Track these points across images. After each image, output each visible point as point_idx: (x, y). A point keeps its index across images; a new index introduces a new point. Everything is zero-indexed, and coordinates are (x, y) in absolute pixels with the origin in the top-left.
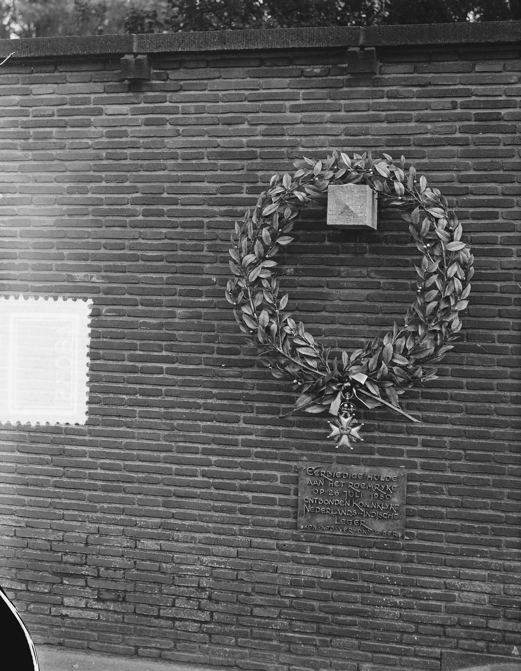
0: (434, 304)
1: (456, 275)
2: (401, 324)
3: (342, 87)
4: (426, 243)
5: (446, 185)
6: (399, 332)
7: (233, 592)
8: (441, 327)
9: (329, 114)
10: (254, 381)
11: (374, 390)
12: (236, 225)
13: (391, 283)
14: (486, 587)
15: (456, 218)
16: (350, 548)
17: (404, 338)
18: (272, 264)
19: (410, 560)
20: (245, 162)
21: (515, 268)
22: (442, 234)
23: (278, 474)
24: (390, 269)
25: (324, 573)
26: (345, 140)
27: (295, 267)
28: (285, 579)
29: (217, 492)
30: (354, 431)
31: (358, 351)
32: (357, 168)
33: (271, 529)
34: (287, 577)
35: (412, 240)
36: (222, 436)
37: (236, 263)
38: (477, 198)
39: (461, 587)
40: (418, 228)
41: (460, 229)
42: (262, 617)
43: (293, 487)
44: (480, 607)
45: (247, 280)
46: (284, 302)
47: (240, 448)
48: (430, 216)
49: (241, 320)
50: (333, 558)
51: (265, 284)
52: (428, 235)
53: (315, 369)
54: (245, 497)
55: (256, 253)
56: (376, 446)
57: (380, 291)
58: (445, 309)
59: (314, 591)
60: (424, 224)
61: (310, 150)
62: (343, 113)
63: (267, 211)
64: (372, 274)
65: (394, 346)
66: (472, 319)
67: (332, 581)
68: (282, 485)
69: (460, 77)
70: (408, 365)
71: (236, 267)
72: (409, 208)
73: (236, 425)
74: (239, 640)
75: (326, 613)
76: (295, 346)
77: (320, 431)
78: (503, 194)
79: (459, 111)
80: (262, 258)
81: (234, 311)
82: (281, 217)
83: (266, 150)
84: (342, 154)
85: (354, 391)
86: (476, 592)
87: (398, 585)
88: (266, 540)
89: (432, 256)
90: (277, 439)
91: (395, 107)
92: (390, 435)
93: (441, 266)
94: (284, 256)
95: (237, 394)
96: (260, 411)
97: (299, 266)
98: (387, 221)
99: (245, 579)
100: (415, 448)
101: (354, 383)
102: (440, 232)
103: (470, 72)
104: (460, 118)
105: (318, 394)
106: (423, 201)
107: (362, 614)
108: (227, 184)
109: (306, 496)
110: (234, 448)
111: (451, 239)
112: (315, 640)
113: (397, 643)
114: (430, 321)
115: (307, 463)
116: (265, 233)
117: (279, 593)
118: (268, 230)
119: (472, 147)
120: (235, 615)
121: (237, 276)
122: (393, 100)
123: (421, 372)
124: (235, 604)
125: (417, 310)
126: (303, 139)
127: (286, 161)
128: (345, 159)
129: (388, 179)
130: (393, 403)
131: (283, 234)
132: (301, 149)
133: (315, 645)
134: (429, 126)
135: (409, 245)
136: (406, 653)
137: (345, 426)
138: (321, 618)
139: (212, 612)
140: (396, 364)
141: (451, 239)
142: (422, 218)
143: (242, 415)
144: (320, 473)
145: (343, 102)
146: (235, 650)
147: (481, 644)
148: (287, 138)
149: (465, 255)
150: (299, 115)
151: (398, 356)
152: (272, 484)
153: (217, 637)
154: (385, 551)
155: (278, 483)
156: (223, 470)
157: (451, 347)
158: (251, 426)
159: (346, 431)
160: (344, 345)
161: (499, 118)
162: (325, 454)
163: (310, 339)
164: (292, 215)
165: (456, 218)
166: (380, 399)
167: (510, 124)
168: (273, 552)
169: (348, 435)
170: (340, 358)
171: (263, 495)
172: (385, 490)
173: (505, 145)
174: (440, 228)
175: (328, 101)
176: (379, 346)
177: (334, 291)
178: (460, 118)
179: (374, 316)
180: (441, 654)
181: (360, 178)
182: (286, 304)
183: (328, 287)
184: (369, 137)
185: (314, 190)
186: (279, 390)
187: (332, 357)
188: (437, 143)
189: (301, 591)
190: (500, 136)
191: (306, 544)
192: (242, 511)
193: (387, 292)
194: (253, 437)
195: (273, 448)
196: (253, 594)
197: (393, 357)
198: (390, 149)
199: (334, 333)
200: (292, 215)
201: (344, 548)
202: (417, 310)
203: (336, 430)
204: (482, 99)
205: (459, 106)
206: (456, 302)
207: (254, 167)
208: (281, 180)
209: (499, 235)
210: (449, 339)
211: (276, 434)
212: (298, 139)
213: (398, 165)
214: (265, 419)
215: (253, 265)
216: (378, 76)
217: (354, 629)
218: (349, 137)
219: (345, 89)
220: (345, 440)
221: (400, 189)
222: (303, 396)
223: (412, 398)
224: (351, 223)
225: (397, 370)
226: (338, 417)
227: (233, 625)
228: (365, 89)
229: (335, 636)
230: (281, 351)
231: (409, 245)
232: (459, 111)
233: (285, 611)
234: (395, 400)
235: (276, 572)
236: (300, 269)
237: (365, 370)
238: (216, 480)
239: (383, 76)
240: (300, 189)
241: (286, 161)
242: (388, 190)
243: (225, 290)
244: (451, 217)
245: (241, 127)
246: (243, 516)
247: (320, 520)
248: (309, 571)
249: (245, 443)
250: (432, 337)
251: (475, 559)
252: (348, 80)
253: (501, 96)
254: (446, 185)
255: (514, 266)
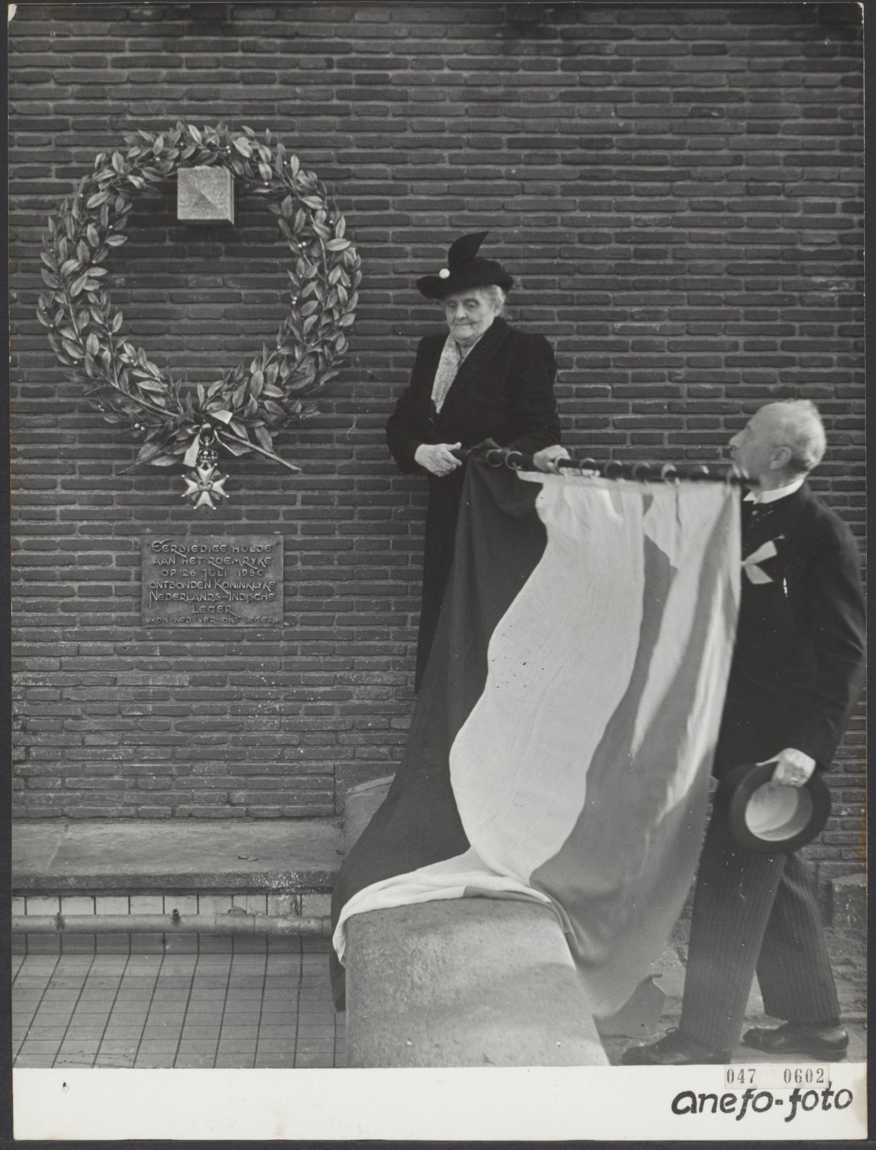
0: (313, 319)
1: (339, 281)
2: (272, 347)
3: (181, 36)
4: (301, 242)
5: (322, 165)
6: (269, 356)
7: (56, 716)
8: (323, 347)
9: (164, 72)
10: (75, 432)
11: (240, 432)
12: (50, 221)
13: (254, 294)
14: (387, 678)
15: (337, 208)
16: (213, 643)
17: (276, 364)
18: (100, 272)
19: (292, 652)
20: (53, 135)
21: (412, 272)
22: (321, 229)
23: (113, 554)
24: (252, 275)
25: (180, 679)
26: (189, 106)
27: (126, 275)
28: (127, 693)
29: (28, 584)
30: (217, 486)
31: (217, 383)
32: (210, 146)
33: (104, 628)
34: (130, 690)
35: (281, 237)
36: (33, 508)
37: (50, 271)
38: (362, 182)
39: (356, 680)
40: (290, 222)
41: (343, 223)
42: (99, 746)
43: (133, 570)
44: (381, 703)
45: (68, 295)
46: (118, 323)
47: (58, 522)
48: (305, 207)
49: (61, 347)
50: (191, 659)
51: (92, 299)
52: (303, 230)
53: (163, 408)
54: (68, 587)
55: (80, 258)
56: (244, 508)
57: (242, 305)
58: (327, 325)
59: (167, 704)
60: (298, 217)
61: (142, 119)
62: (184, 70)
63: (93, 201)
64: (230, 283)
65: (265, 374)
66: (359, 338)
67: (191, 688)
68: (118, 568)
69: (336, 28)
70: (282, 398)
71: (52, 277)
72: (277, 197)
73: (51, 492)
74: (67, 780)
75: (184, 731)
76: (134, 381)
77: (167, 493)
78: (394, 178)
79: (335, 71)
80: (87, 265)
81: (51, 338)
82: (112, 209)
83: (81, 118)
84: (191, 127)
85: (216, 433)
86: (377, 684)
87: (277, 685)
88: (99, 644)
89: (309, 257)
90: (110, 508)
91: (253, 64)
92: (260, 492)
93: (321, 270)
94: (115, 261)
95: (52, 450)
96: (84, 471)
97: (132, 275)
98: (247, 213)
99: (73, 698)
100: (293, 508)
101: (216, 423)
102: (318, 228)
103: (348, 21)
104: (338, 80)
105: (167, 441)
106: (296, 188)
107: (231, 728)
108: (28, 165)
109: (153, 580)
110: (50, 523)
111: (332, 236)
112: (170, 768)
113: (278, 760)
114: (308, 341)
115: (152, 537)
116: (91, 230)
117: (120, 713)
118: (95, 227)
119: (354, 118)
120: (61, 747)
121: (52, 289)
122: (250, 55)
123: (300, 407)
124: (59, 732)
125: (294, 329)
126: (132, 104)
127: (110, 134)
128: (195, 133)
129: (250, 160)
130: (266, 446)
131: (113, 233)
132: (129, 118)
133: (171, 775)
134: (298, 90)
135: (277, 244)
136: (290, 772)
137: (204, 479)
138: (178, 738)
139: (28, 747)
140: (268, 398)
141: (332, 236)
142: (296, 210)
143: (60, 478)
144: (169, 548)
145: (184, 55)
146: (62, 794)
147: (384, 750)
148: (110, 103)
149: (350, 256)
150: (126, 72)
151: (270, 386)
152: (104, 568)
153: (36, 780)
154: (258, 644)
155: (113, 566)
156: (35, 554)
157: (336, 373)
158: (73, 492)
159: (206, 486)
160: (195, 378)
161: (385, 81)
162: (175, 523)
163: (154, 370)
164: (125, 206)
165: (337, 208)
166: (248, 443)
167: (400, 89)
168: (109, 658)
169: (210, 491)
170: (195, 395)
171: (93, 583)
172: (256, 564)
173: (394, 115)
174: (318, 221)
175: (164, 54)
176: (244, 376)
177: (179, 307)
178: (338, 80)
179: (234, 338)
180: (334, 768)
181: (214, 159)
182: (119, 324)
183: (172, 301)
184: (220, 102)
185: (154, 174)
186: (110, 442)
187: (183, 393)
188: (309, 112)
189: (150, 707)
190: (389, 104)
191: (153, 644)
192: (65, 608)
193: (250, 307)
194: (76, 507)
195: (105, 520)
196: (84, 716)
197: (264, 389)
198: (249, 118)
199: (182, 362)
200: (125, 206)
201: (204, 644)
202: (294, 329)
203: (193, 486)
204: (364, 56)
205: (335, 64)
206: (341, 316)
207: (66, 141)
208: (110, 161)
209: (391, 230)
210: (334, 364)
211: (109, 501)
212: (125, 104)
213: (263, 141)
214: (91, 482)
215: (76, 275)
216: (229, 22)
217: (224, 748)
218: (193, 102)
219: (186, 38)
220: (205, 498)
221: (267, 173)
222: (148, 445)
223: (286, 442)
224: (209, 217)
225: (270, 405)
226: (195, 469)
227: (57, 761)
228: (212, 38)
229: (197, 760)
230: (117, 386)
231: (277, 244)
232: (335, 71)
233: (129, 734)
234: (268, 443)
235: (115, 685)
236: (134, 279)
237: (228, 407)
238: (27, 569)
239: (237, 23)
240: (137, 173)
241: (110, 134)
242: (251, 173)
243: (34, 311)
244: (331, 208)
245: (45, 86)
246: (67, 614)
247: (171, 610)
248: (157, 681)
249: (65, 516)
250: (312, 361)
251: (372, 643)
252: (189, 26)
253: (387, 53)
254: (322, 165)
255: (409, 269)
